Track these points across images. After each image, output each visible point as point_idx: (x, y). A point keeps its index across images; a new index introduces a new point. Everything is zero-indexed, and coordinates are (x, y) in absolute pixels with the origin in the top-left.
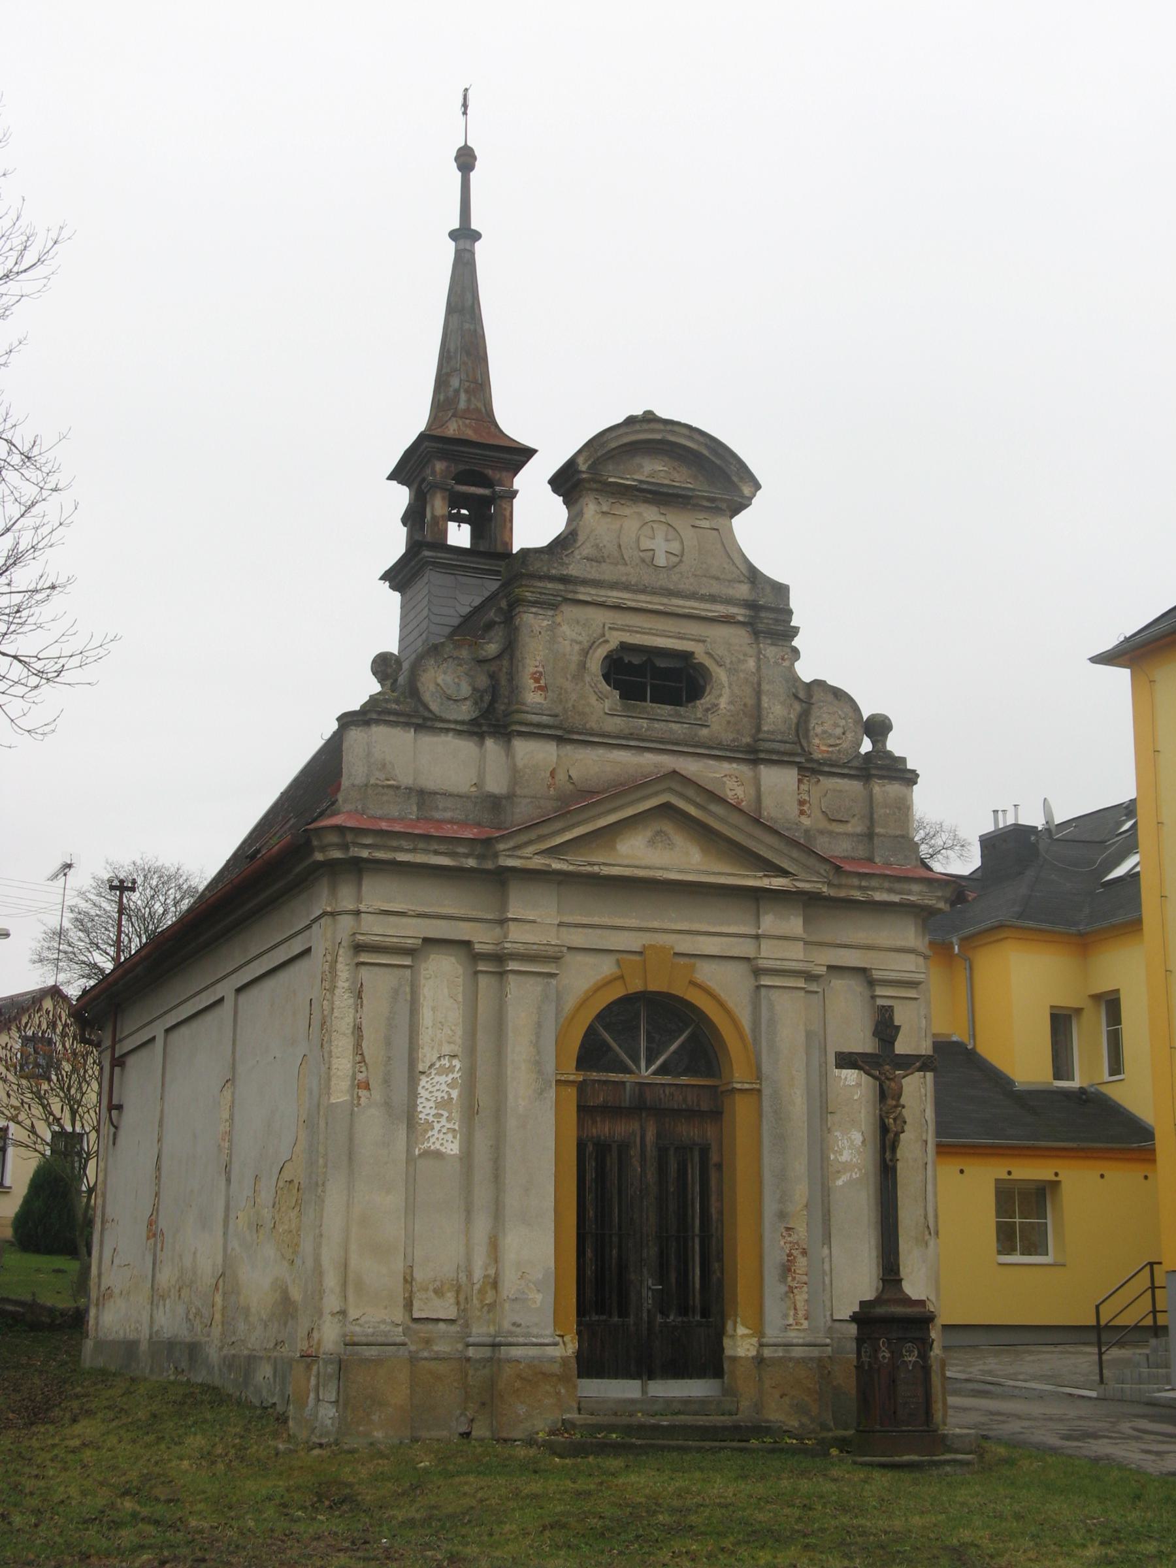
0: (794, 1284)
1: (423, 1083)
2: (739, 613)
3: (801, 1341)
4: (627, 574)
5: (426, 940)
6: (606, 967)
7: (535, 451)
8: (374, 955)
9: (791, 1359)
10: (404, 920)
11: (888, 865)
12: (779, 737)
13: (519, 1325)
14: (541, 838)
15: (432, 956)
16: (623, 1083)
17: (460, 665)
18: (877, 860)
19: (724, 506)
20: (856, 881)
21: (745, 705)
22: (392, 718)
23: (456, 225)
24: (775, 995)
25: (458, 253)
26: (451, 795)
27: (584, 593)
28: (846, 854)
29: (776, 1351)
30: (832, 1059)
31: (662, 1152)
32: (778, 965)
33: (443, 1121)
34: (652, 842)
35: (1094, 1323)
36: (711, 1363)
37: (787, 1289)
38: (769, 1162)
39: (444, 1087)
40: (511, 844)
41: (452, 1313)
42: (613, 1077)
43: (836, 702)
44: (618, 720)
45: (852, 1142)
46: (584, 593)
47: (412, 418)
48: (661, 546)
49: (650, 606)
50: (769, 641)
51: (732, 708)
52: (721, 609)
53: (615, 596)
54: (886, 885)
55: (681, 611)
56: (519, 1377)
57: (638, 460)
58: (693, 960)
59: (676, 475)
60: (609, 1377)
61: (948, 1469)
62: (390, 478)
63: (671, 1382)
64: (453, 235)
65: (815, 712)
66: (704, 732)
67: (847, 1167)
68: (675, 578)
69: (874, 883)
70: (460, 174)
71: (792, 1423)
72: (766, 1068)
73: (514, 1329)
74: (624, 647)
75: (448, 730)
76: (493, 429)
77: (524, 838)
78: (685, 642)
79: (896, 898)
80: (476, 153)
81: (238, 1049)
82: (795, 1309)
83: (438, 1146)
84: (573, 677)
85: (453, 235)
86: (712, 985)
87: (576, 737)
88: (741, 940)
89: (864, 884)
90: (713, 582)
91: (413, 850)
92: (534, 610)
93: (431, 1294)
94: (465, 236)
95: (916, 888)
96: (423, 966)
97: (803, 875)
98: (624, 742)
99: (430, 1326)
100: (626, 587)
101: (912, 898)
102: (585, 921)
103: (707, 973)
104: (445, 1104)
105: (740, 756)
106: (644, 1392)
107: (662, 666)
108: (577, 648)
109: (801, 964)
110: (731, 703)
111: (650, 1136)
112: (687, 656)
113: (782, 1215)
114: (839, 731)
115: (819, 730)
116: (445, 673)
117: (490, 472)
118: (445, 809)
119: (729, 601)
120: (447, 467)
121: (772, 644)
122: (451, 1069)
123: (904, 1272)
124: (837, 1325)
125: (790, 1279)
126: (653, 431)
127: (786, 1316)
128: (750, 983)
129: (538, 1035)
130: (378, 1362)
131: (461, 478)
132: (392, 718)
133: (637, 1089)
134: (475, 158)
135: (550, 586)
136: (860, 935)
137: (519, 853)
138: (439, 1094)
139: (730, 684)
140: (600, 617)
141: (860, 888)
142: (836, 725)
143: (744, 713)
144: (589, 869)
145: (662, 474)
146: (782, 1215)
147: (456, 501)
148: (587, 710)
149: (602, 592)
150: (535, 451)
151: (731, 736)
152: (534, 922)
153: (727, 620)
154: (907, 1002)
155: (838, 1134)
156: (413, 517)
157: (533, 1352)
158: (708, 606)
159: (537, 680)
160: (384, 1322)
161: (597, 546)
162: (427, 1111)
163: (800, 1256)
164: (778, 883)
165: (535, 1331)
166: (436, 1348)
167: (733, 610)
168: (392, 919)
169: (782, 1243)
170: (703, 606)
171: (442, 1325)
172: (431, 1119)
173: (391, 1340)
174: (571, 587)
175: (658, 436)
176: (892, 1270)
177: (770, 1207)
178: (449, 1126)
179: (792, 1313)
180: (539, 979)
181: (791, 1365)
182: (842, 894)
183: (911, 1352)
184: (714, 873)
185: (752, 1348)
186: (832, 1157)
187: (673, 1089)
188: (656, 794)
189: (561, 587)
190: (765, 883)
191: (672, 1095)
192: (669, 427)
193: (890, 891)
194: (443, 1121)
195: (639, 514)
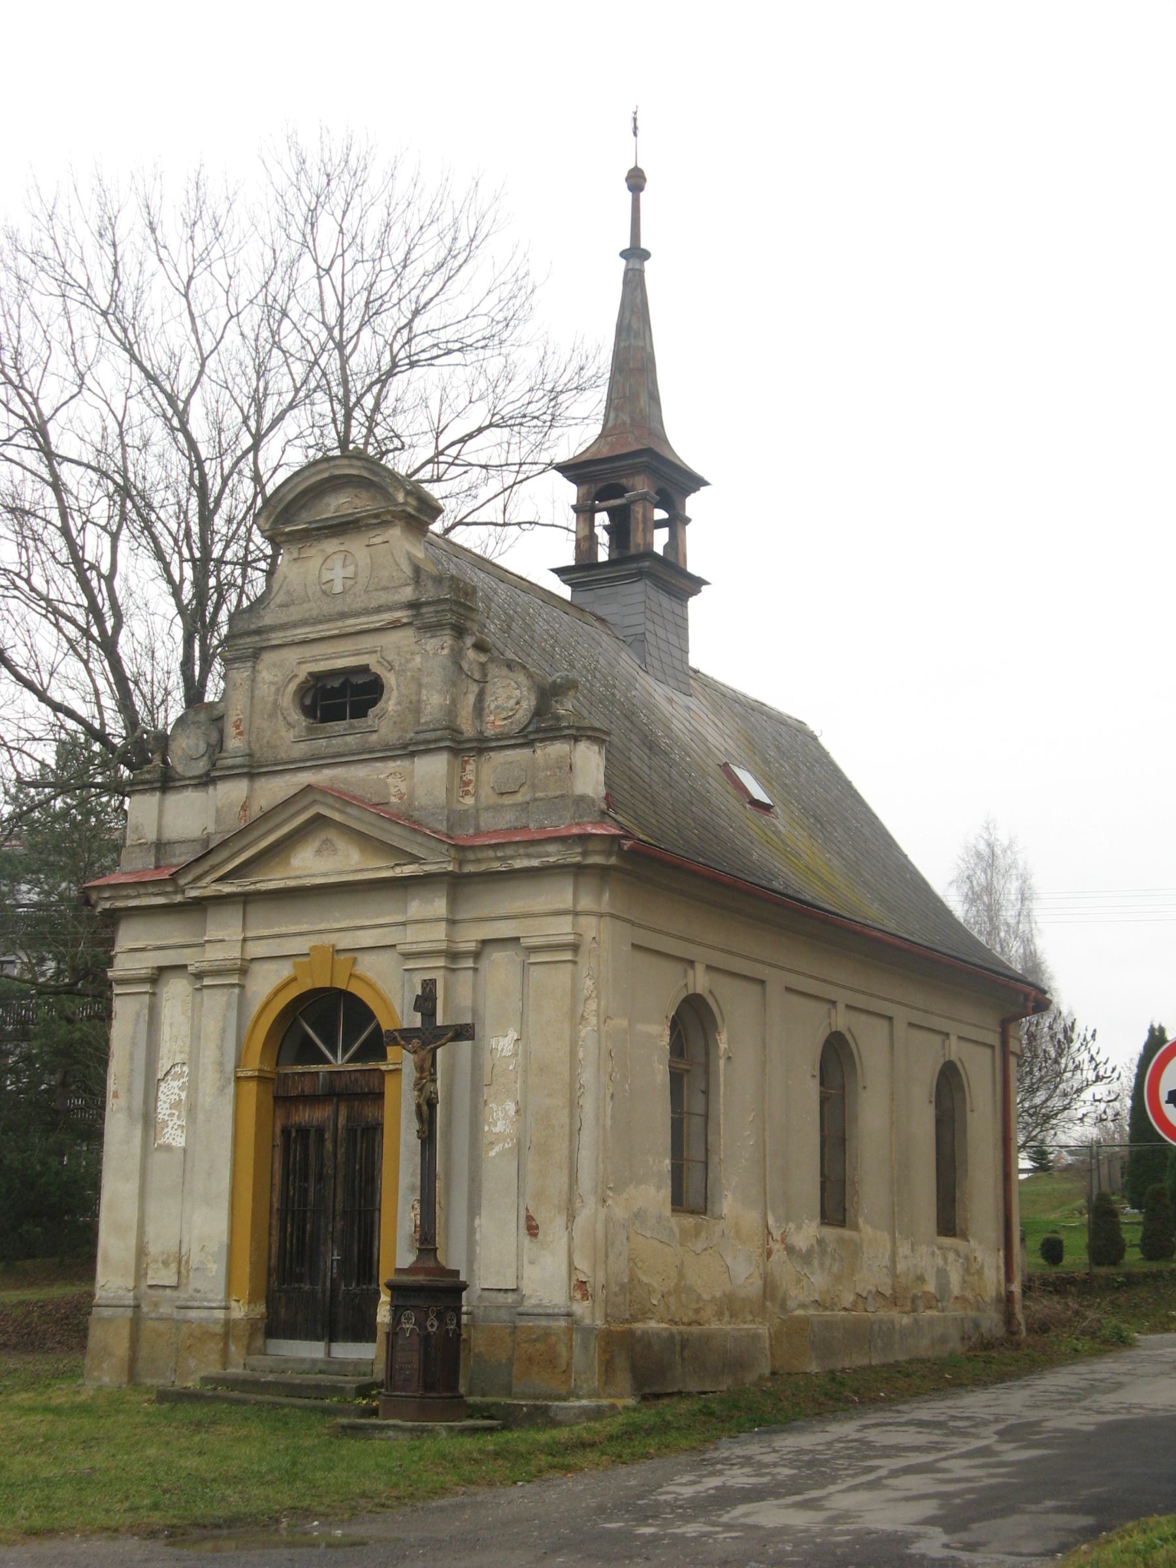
1: (161, 1089)
2: (403, 615)
4: (310, 610)
5: (484, 942)
6: (285, 971)
8: (124, 987)
10: (145, 954)
11: (542, 828)
12: (432, 726)
13: (199, 1291)
14: (213, 868)
15: (172, 981)
16: (317, 1073)
17: (199, 728)
18: (531, 826)
19: (389, 518)
20: (491, 853)
21: (411, 702)
22: (140, 787)
23: (626, 245)
26: (184, 842)
27: (276, 638)
28: (509, 825)
31: (351, 1131)
33: (175, 1118)
34: (319, 852)
39: (176, 1091)
40: (190, 878)
41: (173, 1281)
42: (314, 1068)
43: (511, 674)
44: (302, 745)
45: (506, 1112)
46: (276, 638)
48: (337, 575)
49: (328, 633)
50: (429, 635)
51: (399, 708)
52: (388, 617)
53: (301, 633)
54: (522, 851)
55: (352, 630)
56: (191, 1335)
57: (327, 500)
58: (355, 955)
59: (357, 502)
60: (300, 1339)
61: (391, 1433)
63: (350, 1345)
64: (624, 254)
65: (489, 688)
66: (374, 737)
67: (500, 1137)
68: (348, 600)
69: (509, 851)
70: (630, 194)
73: (195, 1294)
74: (316, 677)
75: (186, 786)
77: (198, 871)
78: (361, 657)
79: (535, 863)
80: (647, 175)
83: (171, 1140)
84: (269, 716)
85: (624, 254)
86: (370, 975)
87: (264, 770)
89: (499, 854)
90: (381, 593)
91: (138, 896)
92: (236, 665)
93: (160, 1265)
94: (635, 254)
95: (551, 848)
96: (165, 990)
97: (431, 859)
98: (356, 758)
99: (160, 1292)
100: (304, 623)
101: (552, 860)
102: (266, 932)
103: (368, 966)
104: (176, 1105)
105: (512, 742)
106: (329, 1353)
107: (360, 682)
108: (273, 688)
110: (399, 703)
111: (342, 1121)
112: (364, 669)
114: (512, 702)
115: (492, 707)
116: (188, 737)
117: (624, 481)
118: (180, 855)
119: (389, 608)
120: (588, 490)
121: (432, 637)
122: (182, 1075)
124: (486, 1293)
126: (321, 472)
129: (222, 1039)
130: (110, 1320)
132: (140, 787)
134: (645, 180)
135: (248, 640)
136: (518, 905)
137: (199, 884)
138: (173, 1097)
139: (398, 685)
140: (291, 656)
141: (498, 859)
142: (509, 698)
143: (410, 711)
144: (252, 887)
145: (345, 506)
148: (278, 743)
149: (289, 633)
151: (396, 735)
152: (222, 941)
153: (396, 625)
154: (561, 965)
155: (493, 1105)
157: (203, 1314)
158: (375, 618)
159: (237, 727)
160: (120, 1288)
161: (288, 591)
162: (164, 1112)
164: (408, 870)
165: (210, 1296)
166: (161, 1310)
167: (398, 614)
168: (138, 955)
170: (371, 619)
171: (168, 1291)
172: (166, 1118)
173: (121, 1303)
174: (264, 636)
175: (326, 475)
176: (426, 1239)
178: (179, 1123)
180: (225, 990)
182: (482, 868)
183: (408, 1319)
184: (372, 869)
186: (486, 1128)
187: (358, 1074)
188: (305, 808)
189: (257, 638)
190: (399, 872)
191: (356, 1080)
192: (332, 463)
193: (529, 856)
194: (175, 1118)
195: (323, 551)
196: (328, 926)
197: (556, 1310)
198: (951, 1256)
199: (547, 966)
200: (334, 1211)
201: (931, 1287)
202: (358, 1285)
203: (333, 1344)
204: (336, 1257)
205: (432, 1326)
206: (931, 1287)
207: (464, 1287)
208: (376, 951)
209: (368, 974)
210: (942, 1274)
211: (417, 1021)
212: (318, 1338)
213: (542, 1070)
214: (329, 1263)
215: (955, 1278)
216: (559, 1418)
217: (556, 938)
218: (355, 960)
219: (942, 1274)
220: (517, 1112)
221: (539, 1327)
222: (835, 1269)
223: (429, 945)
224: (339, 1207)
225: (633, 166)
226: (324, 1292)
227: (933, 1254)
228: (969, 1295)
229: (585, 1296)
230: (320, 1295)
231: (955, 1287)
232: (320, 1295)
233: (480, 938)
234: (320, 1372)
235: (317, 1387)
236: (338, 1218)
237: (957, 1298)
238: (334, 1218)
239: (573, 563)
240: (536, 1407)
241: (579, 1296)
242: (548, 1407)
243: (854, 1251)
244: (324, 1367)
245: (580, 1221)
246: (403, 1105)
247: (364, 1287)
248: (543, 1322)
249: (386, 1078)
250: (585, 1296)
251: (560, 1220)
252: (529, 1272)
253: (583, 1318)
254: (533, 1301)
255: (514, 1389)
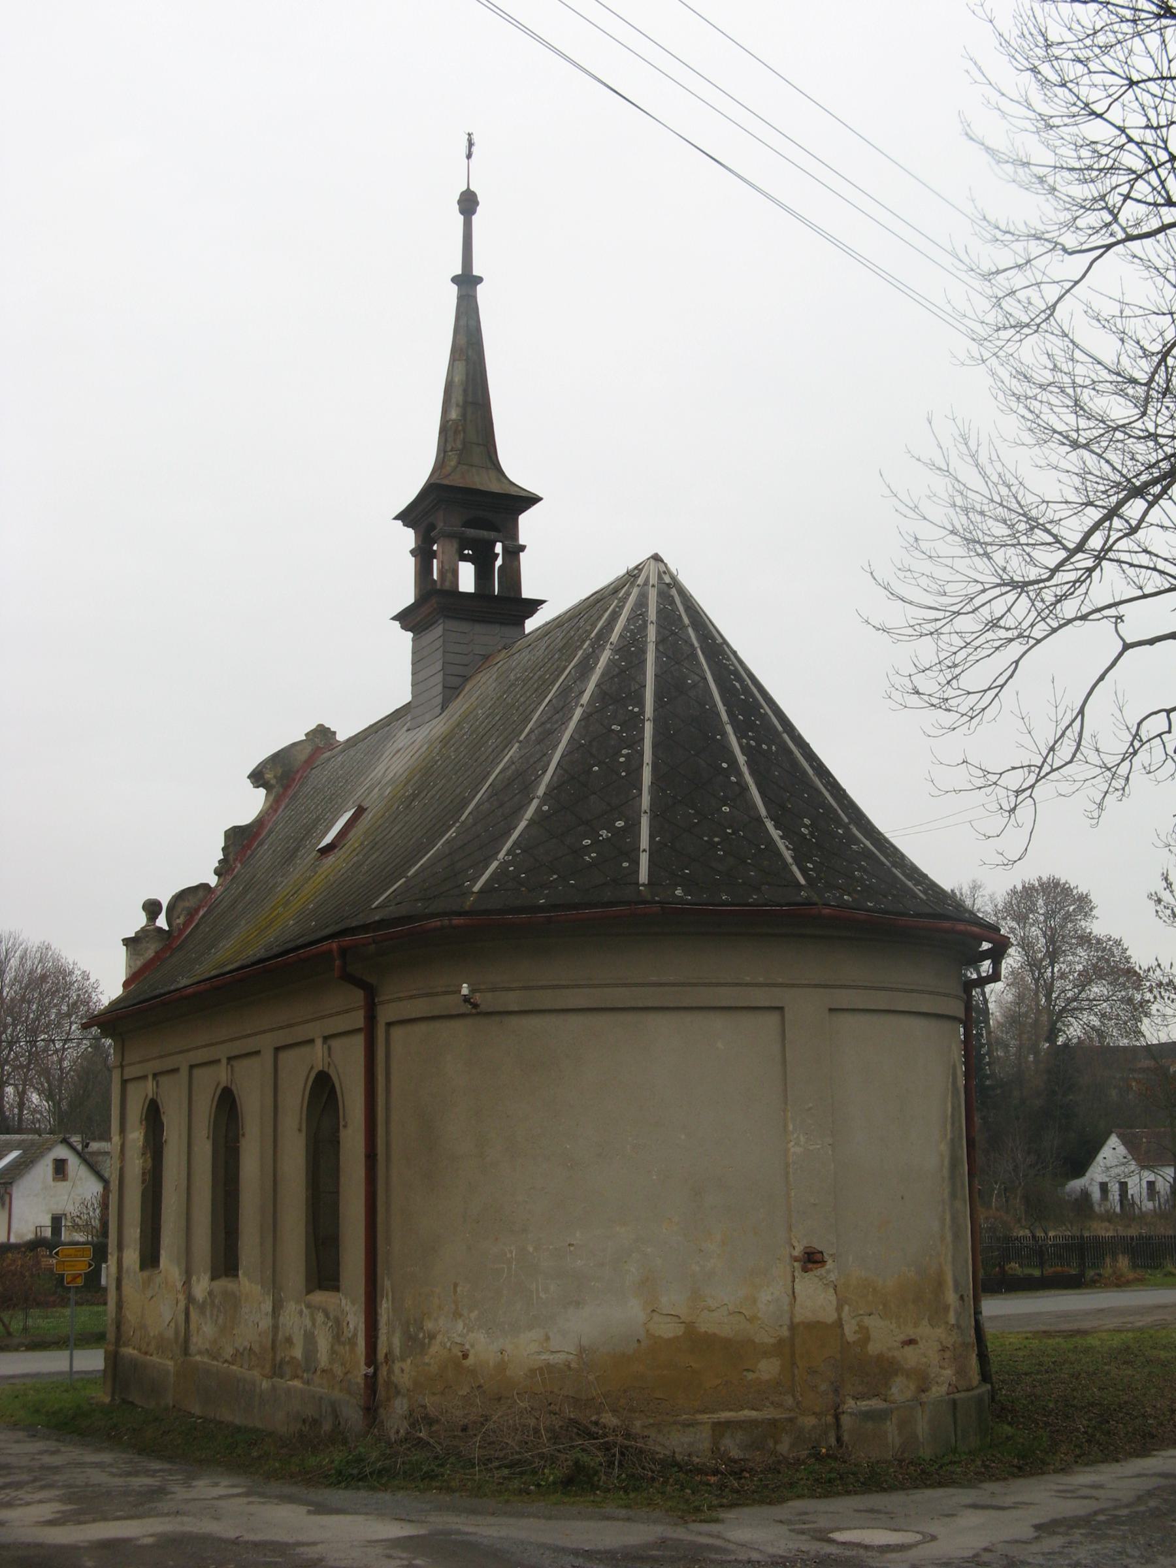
7: (541, 499)
25: (461, 298)
35: (67, 1369)
47: (414, 464)
62: (396, 518)
64: (455, 280)
76: (298, 748)
80: (479, 199)
81: (413, 1016)
94: (467, 282)
131: (469, 524)
134: (477, 203)
147: (464, 543)
150: (541, 499)
156: (423, 555)
198: (320, 1317)
201: (298, 1352)
206: (298, 1352)
210: (310, 1338)
215: (323, 1344)
219: (310, 1338)
222: (220, 1321)
225: (465, 188)
227: (301, 1312)
228: (338, 1370)
231: (323, 1356)
237: (323, 1371)
239: (524, 596)
243: (232, 1302)
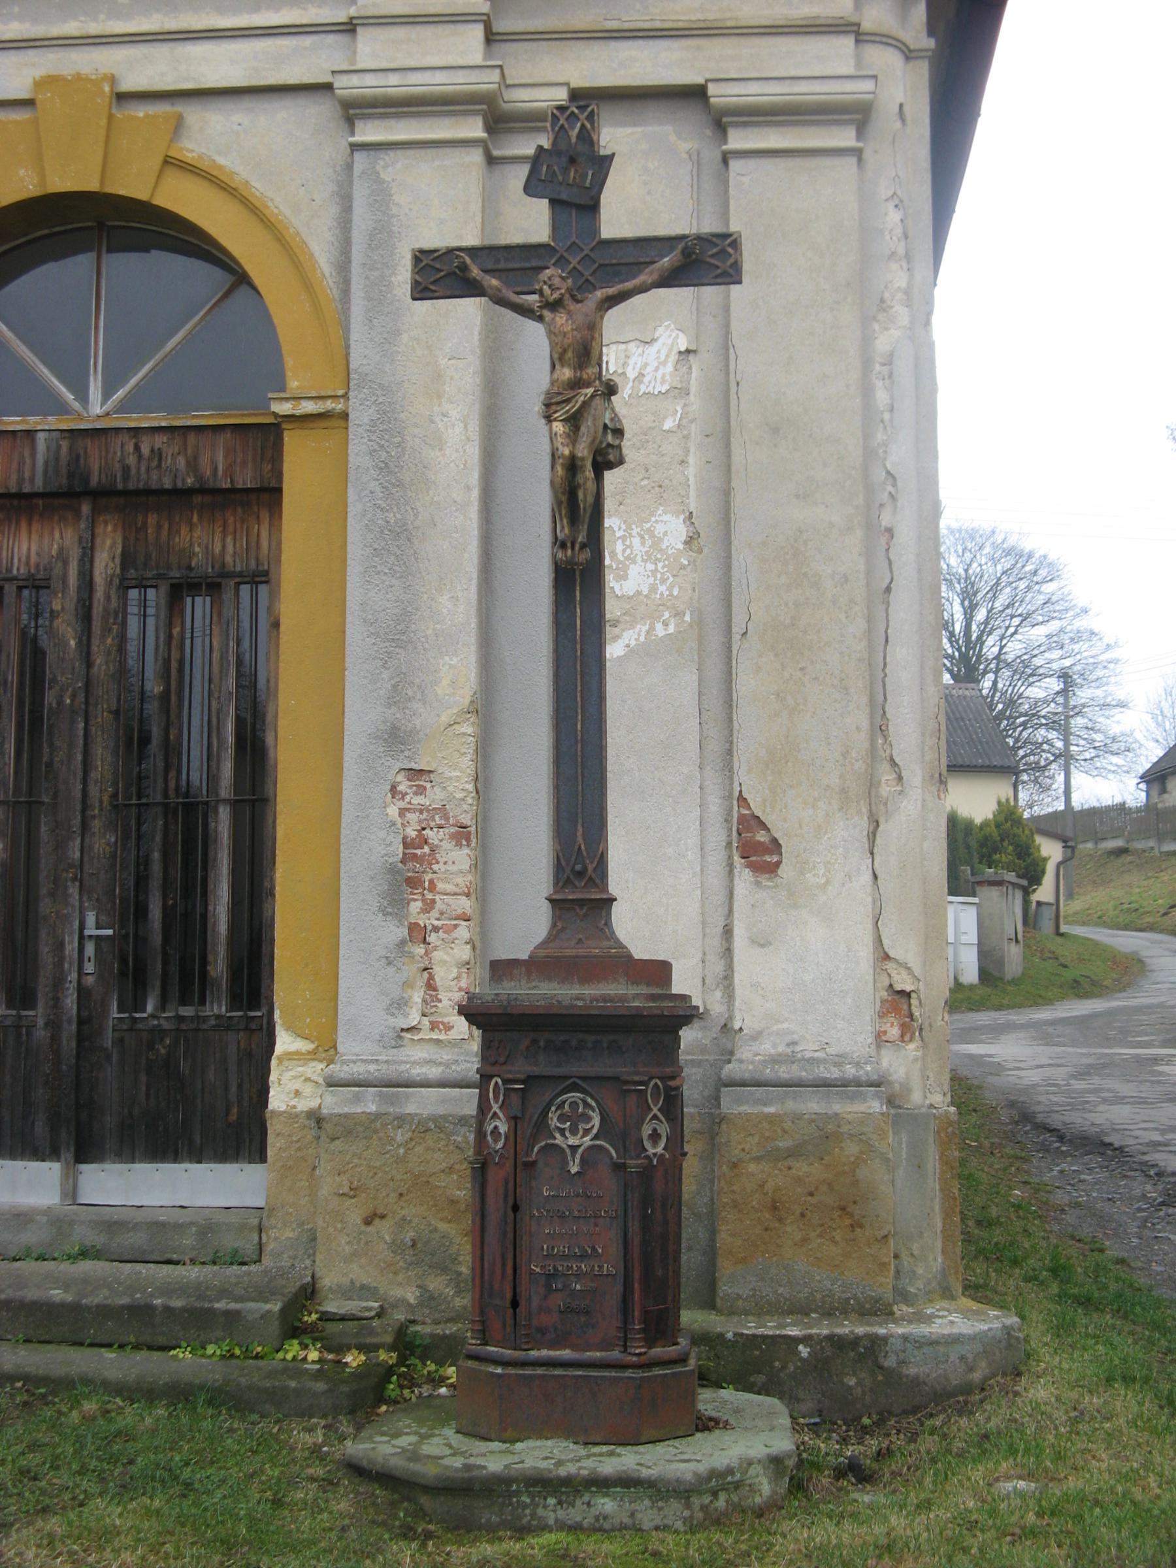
0: (430, 920)
3: (434, 1072)
9: (401, 1120)
16: (30, 434)
24: (393, 168)
29: (357, 1099)
30: (403, 275)
32: (393, 86)
36: (239, 1131)
37: (404, 932)
38: (362, 592)
45: (657, 542)
58: (179, 107)
61: (606, 1504)
71: (397, 1292)
72: (362, 354)
82: (431, 986)
86: (230, 162)
88: (308, 41)
103: (213, 135)
106: (71, 1192)
109: (474, 77)
113: (396, 738)
123: (618, 880)
125: (416, 906)
127: (401, 1004)
128: (334, 147)
133: (65, 444)
146: (396, 738)
163: (447, 845)
169: (393, 811)
177: (362, 715)
179: (417, 997)
181: (400, 1136)
185: (307, 1089)
187: (160, 440)
196: (93, 28)
197: (850, 1071)
199: (781, 163)
200: (85, 807)
202: (163, 1005)
203: (83, 1167)
204: (91, 931)
205: (655, 1137)
207: (684, 1014)
208: (247, 102)
209: (221, 161)
211: (530, 221)
212: (36, 1153)
213: (775, 431)
214: (71, 947)
216: (912, 1371)
217: (817, 87)
218: (179, 124)
220: (689, 541)
221: (797, 1117)
223: (439, 77)
224: (99, 794)
226: (54, 1025)
229: (908, 1029)
230: (41, 1034)
232: (41, 1034)
233: (578, 82)
234: (84, 1254)
235: (140, 1312)
236: (96, 825)
238: (85, 826)
240: (839, 1344)
241: (894, 1032)
242: (876, 1343)
244: (96, 1239)
245: (893, 831)
246: (354, 509)
247: (187, 1011)
248: (813, 1105)
249: (287, 437)
250: (908, 1029)
251: (847, 831)
252: (748, 963)
253: (907, 1089)
254: (767, 1047)
255: (724, 1289)
